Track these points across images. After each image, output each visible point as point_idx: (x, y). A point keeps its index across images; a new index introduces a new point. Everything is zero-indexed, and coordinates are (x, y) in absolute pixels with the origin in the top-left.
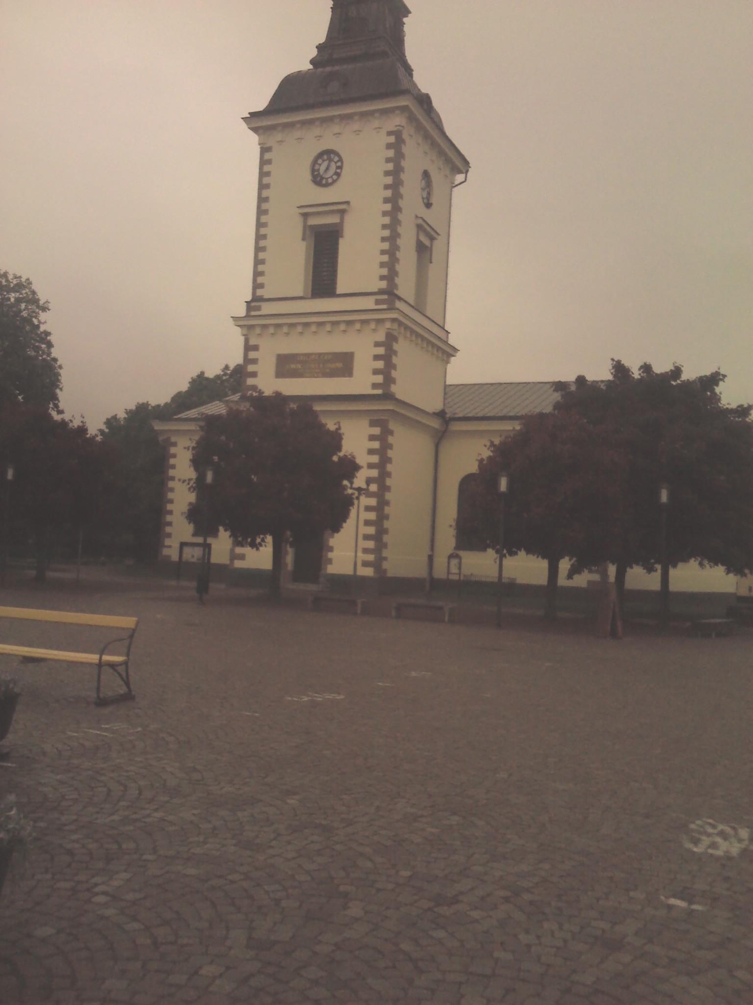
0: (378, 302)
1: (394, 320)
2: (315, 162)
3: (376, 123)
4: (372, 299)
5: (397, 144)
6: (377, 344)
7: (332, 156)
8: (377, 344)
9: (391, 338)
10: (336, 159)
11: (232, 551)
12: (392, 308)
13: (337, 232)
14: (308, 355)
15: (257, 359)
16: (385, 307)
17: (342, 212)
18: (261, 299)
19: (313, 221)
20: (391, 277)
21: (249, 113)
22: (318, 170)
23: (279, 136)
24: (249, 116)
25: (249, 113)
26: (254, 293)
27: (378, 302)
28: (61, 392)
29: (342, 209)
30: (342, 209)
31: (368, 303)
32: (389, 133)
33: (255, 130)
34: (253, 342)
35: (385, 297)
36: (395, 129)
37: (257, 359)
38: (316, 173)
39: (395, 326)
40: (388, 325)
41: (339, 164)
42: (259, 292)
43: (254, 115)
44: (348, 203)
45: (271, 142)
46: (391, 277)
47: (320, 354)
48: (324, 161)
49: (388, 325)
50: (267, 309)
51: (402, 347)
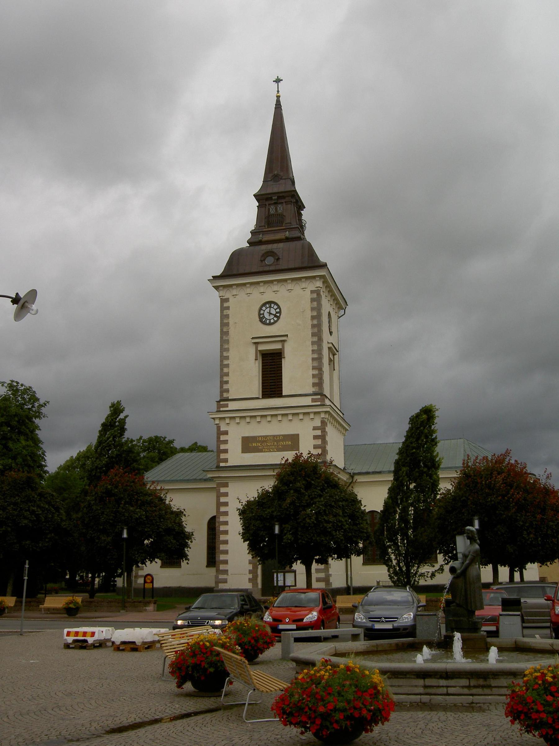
0: (313, 400)
1: (326, 412)
2: (260, 309)
3: (304, 285)
4: (310, 398)
5: (316, 298)
6: (315, 428)
7: (272, 305)
8: (315, 428)
9: (323, 423)
10: (276, 307)
11: (217, 577)
12: (323, 405)
13: (281, 353)
14: (266, 437)
15: (228, 502)
16: (319, 403)
17: (283, 341)
18: (228, 400)
19: (261, 348)
20: (319, 384)
21: (212, 277)
22: (263, 314)
23: (234, 292)
24: (212, 278)
25: (212, 277)
26: (221, 395)
27: (313, 400)
28: (228, 385)
29: (283, 339)
30: (283, 339)
31: (308, 401)
32: (312, 292)
33: (217, 288)
34: (223, 428)
35: (319, 397)
36: (316, 289)
37: (228, 502)
38: (261, 316)
39: (327, 416)
40: (323, 415)
41: (278, 310)
42: (225, 395)
43: (215, 277)
44: (287, 336)
45: (227, 294)
46: (319, 384)
47: (274, 436)
48: (266, 308)
49: (323, 415)
50: (232, 406)
51: (329, 429)
